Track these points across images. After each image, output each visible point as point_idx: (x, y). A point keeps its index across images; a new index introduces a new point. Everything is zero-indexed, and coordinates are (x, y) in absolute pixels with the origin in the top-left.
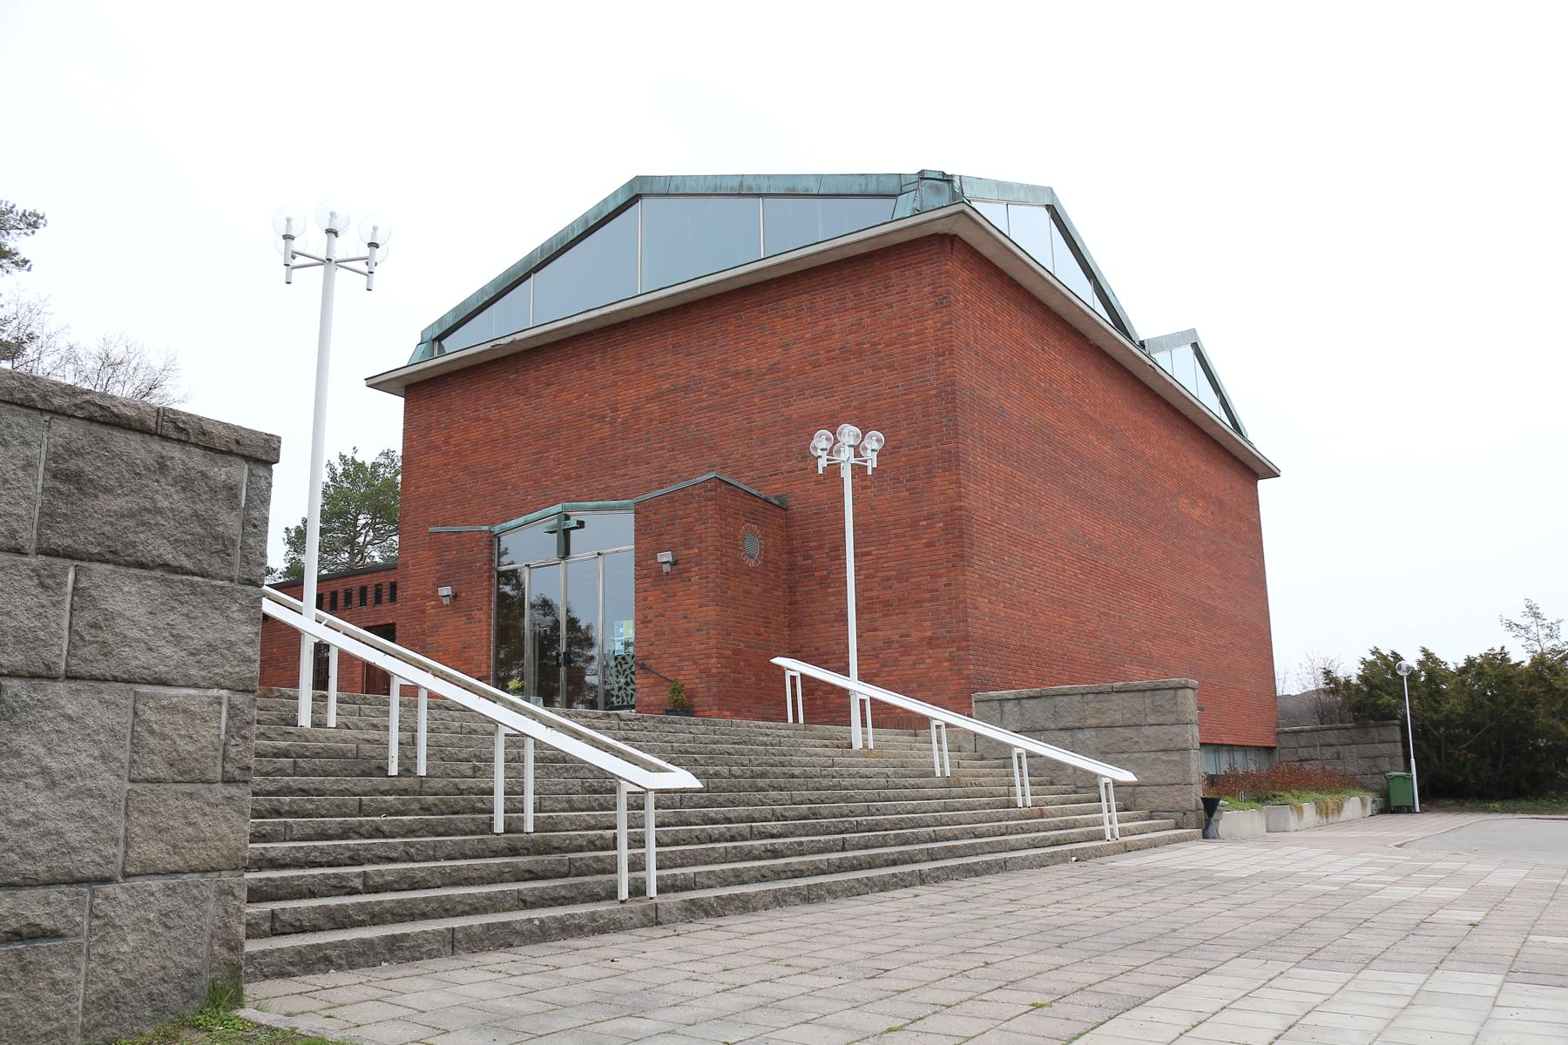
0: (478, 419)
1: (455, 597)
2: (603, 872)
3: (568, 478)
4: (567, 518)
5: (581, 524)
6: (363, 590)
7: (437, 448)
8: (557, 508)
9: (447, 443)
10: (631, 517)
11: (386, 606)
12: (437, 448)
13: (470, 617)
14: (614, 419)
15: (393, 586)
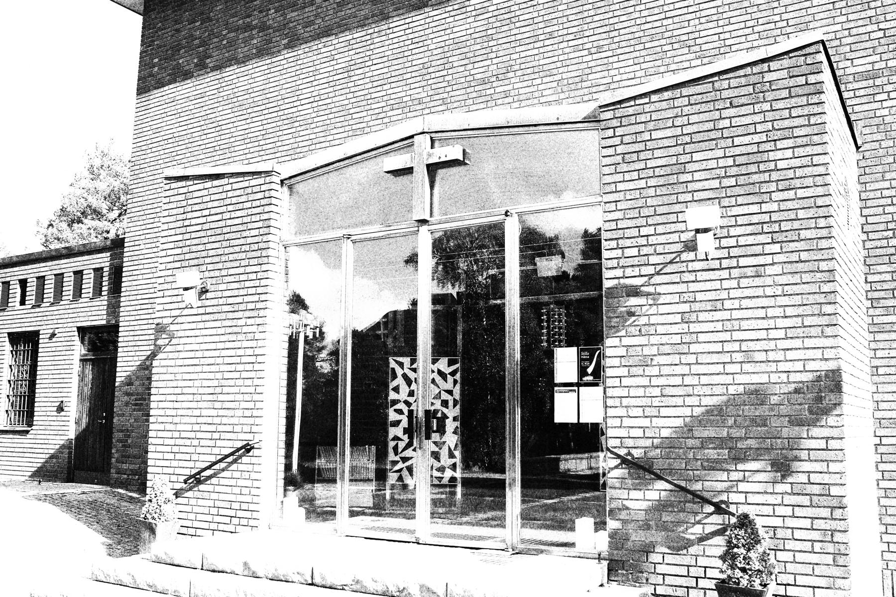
0: (248, 27)
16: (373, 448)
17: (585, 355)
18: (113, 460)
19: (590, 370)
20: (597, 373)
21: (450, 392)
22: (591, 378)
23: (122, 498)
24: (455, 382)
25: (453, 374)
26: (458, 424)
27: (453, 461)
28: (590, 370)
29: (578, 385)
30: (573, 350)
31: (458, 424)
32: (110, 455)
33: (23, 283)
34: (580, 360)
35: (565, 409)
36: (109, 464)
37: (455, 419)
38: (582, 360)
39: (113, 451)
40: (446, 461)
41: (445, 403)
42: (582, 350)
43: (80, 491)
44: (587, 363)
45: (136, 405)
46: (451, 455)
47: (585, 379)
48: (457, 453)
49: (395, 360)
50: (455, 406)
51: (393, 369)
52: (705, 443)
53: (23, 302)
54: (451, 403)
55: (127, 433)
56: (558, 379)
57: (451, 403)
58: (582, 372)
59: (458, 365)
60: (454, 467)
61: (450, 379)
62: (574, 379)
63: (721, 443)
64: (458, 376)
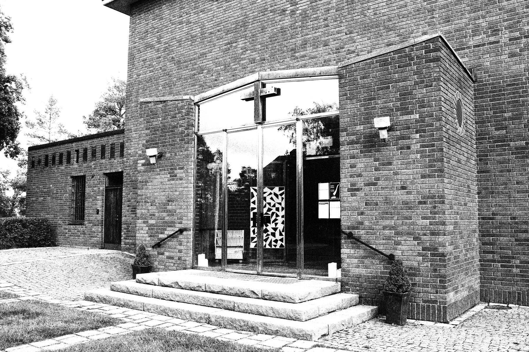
0: (181, 23)
1: (160, 157)
2: (266, 262)
3: (253, 61)
4: (264, 86)
5: (278, 92)
6: (103, 147)
7: (152, 47)
8: (255, 77)
9: (159, 42)
10: (335, 83)
11: (116, 161)
12: (152, 47)
13: (173, 176)
14: (293, 12)
15: (122, 146)
16: (243, 231)
17: (333, 187)
18: (122, 238)
19: (334, 194)
20: (338, 195)
21: (280, 204)
22: (335, 197)
23: (127, 256)
24: (282, 198)
25: (281, 195)
26: (284, 219)
27: (281, 237)
28: (334, 194)
29: (329, 201)
30: (327, 185)
31: (284, 219)
32: (121, 236)
33: (77, 151)
34: (330, 189)
35: (323, 212)
36: (121, 240)
37: (283, 217)
38: (331, 189)
39: (122, 233)
40: (278, 237)
41: (277, 209)
42: (331, 184)
43: (107, 253)
44: (333, 190)
45: (132, 211)
46: (281, 234)
47: (332, 198)
48: (284, 233)
49: (254, 189)
50: (282, 210)
51: (252, 193)
52: (384, 228)
53: (77, 162)
54: (280, 209)
55: (128, 224)
56: (321, 197)
57: (280, 209)
58: (331, 194)
59: (284, 190)
60: (281, 240)
61: (280, 197)
62: (327, 198)
63: (391, 228)
64: (284, 196)
